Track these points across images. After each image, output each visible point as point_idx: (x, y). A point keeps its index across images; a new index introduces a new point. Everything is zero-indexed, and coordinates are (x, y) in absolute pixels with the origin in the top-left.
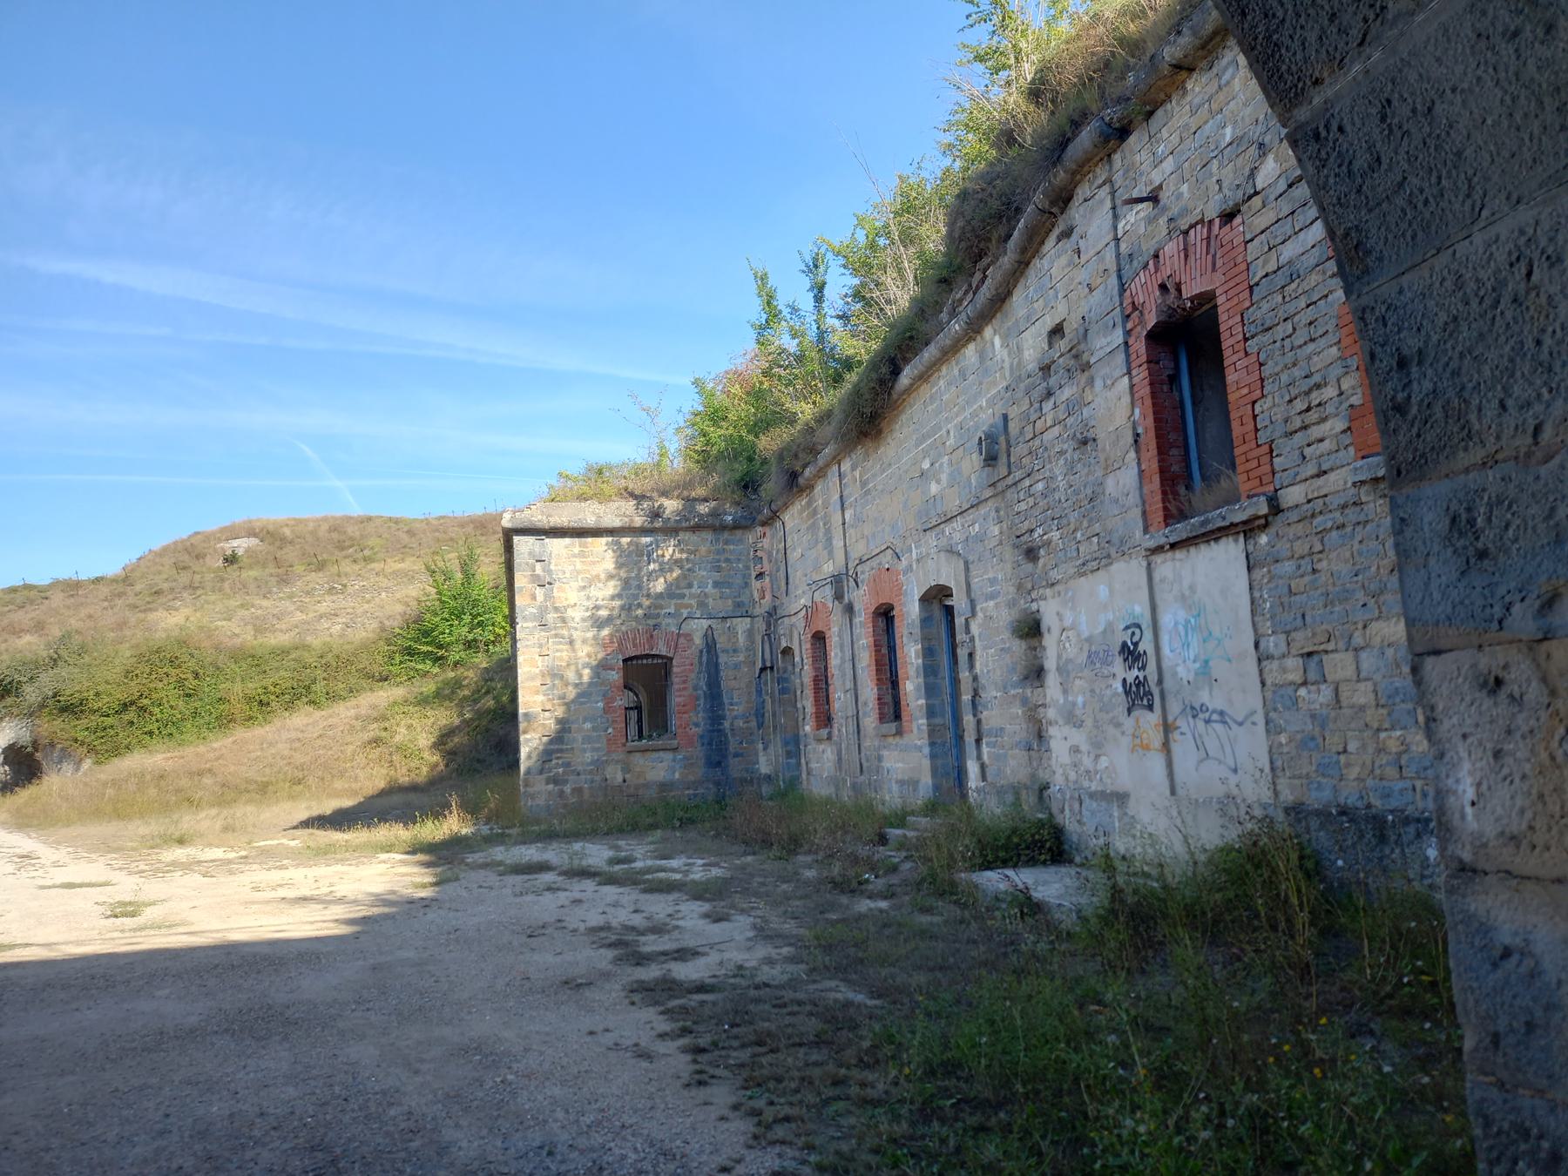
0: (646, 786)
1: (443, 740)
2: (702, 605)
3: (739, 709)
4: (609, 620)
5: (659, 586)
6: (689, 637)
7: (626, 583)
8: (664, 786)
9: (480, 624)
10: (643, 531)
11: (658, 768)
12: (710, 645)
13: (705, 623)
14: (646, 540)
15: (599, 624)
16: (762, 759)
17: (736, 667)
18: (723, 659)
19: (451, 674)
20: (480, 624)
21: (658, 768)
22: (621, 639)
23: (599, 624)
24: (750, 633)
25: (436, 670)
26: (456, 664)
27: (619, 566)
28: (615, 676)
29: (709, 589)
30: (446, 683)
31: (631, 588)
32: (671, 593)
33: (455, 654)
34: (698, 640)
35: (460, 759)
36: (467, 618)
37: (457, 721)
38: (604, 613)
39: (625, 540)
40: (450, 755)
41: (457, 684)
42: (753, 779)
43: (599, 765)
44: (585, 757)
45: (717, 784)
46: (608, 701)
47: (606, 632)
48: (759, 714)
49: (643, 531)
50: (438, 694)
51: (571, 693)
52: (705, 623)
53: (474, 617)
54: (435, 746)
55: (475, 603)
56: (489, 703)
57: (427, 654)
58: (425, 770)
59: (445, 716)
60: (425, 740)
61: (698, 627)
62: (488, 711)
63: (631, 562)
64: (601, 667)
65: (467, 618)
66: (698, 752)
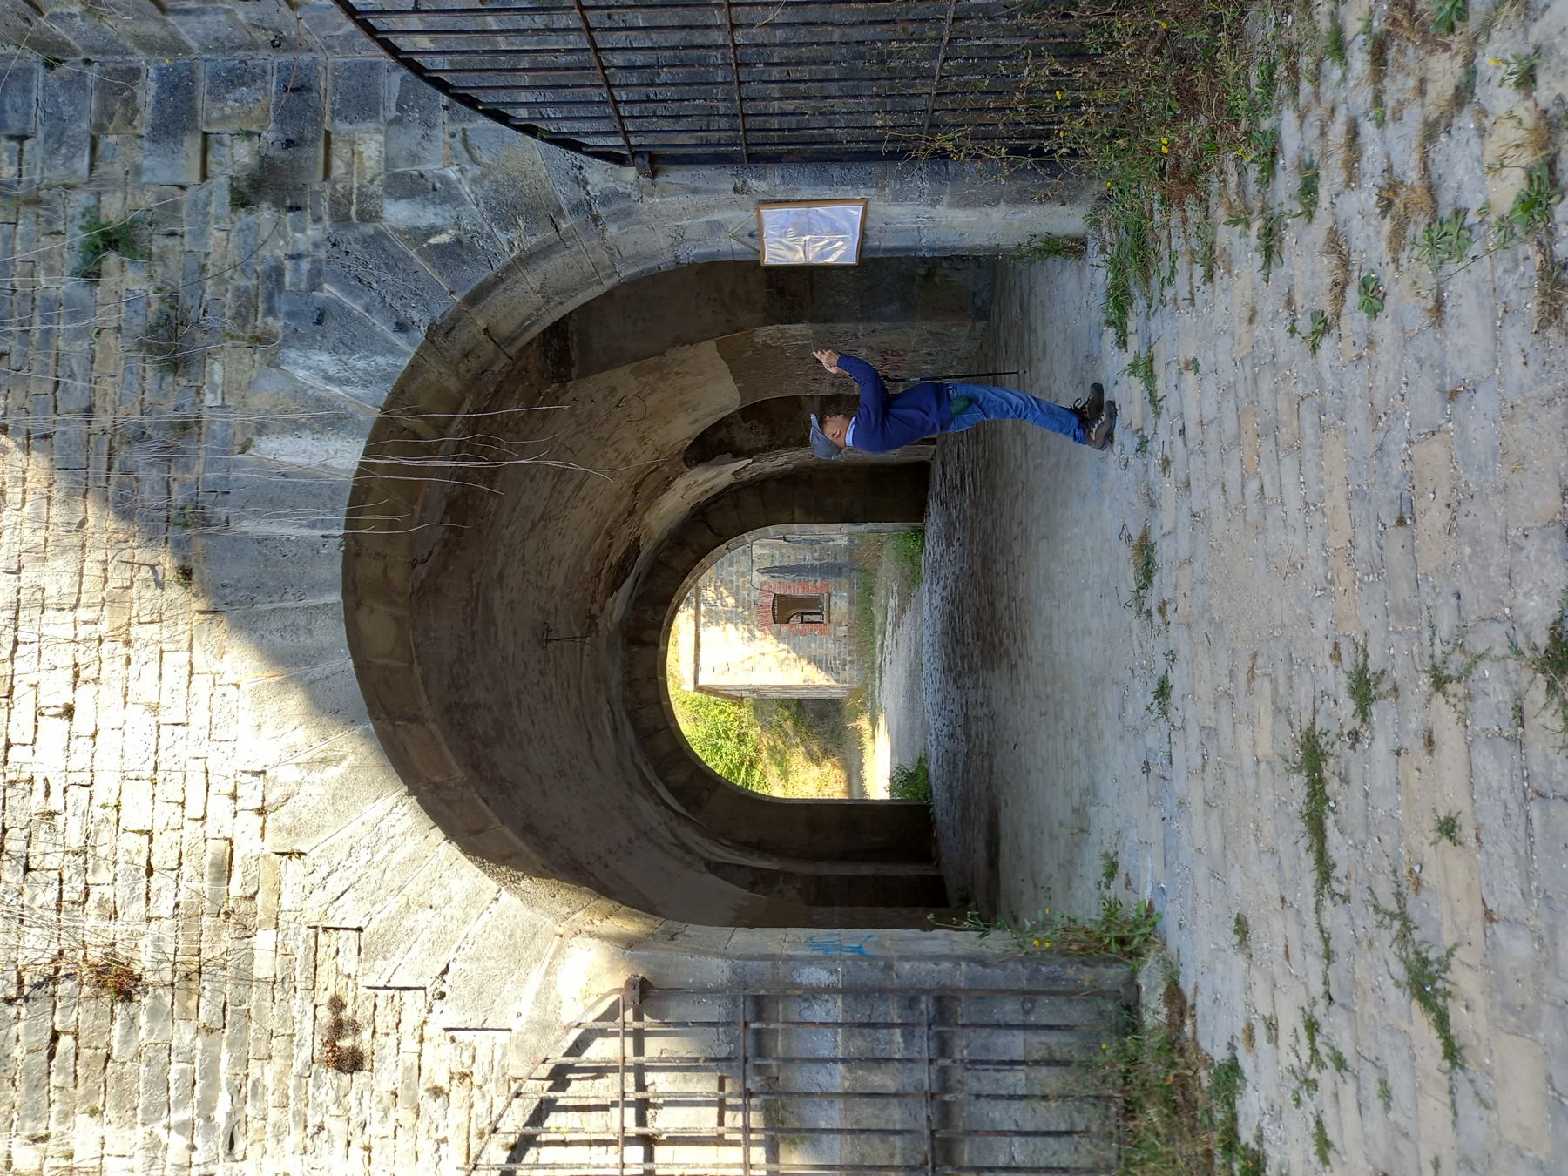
0: (850, 612)
1: (812, 758)
2: (743, 575)
3: (808, 556)
4: (750, 631)
5: (731, 601)
6: (763, 584)
7: (728, 620)
8: (851, 602)
9: (725, 732)
10: (697, 608)
11: (840, 606)
12: (768, 571)
13: (755, 573)
14: (703, 608)
15: (752, 637)
16: (839, 542)
17: (782, 555)
18: (777, 564)
19: (765, 754)
20: (725, 732)
21: (840, 606)
22: (762, 626)
23: (752, 637)
24: (762, 546)
25: (760, 767)
26: (756, 750)
27: (717, 624)
28: (784, 628)
29: (734, 569)
30: (771, 757)
31: (731, 618)
32: (735, 595)
33: (748, 750)
34: (765, 578)
35: (830, 746)
36: (720, 742)
37: (802, 749)
38: (746, 634)
39: (703, 620)
40: (826, 753)
41: (772, 750)
42: (849, 549)
43: (836, 640)
44: (831, 648)
45: (852, 569)
46: (799, 633)
47: (757, 633)
48: (812, 543)
49: (697, 608)
50: (780, 764)
51: (793, 655)
52: (755, 573)
53: (719, 736)
54: (819, 765)
55: (709, 736)
56: (788, 725)
57: (748, 773)
58: (837, 771)
59: (797, 758)
60: (814, 771)
61: (757, 578)
62: (795, 724)
63: (715, 617)
64: (778, 636)
65: (720, 742)
66: (832, 581)
